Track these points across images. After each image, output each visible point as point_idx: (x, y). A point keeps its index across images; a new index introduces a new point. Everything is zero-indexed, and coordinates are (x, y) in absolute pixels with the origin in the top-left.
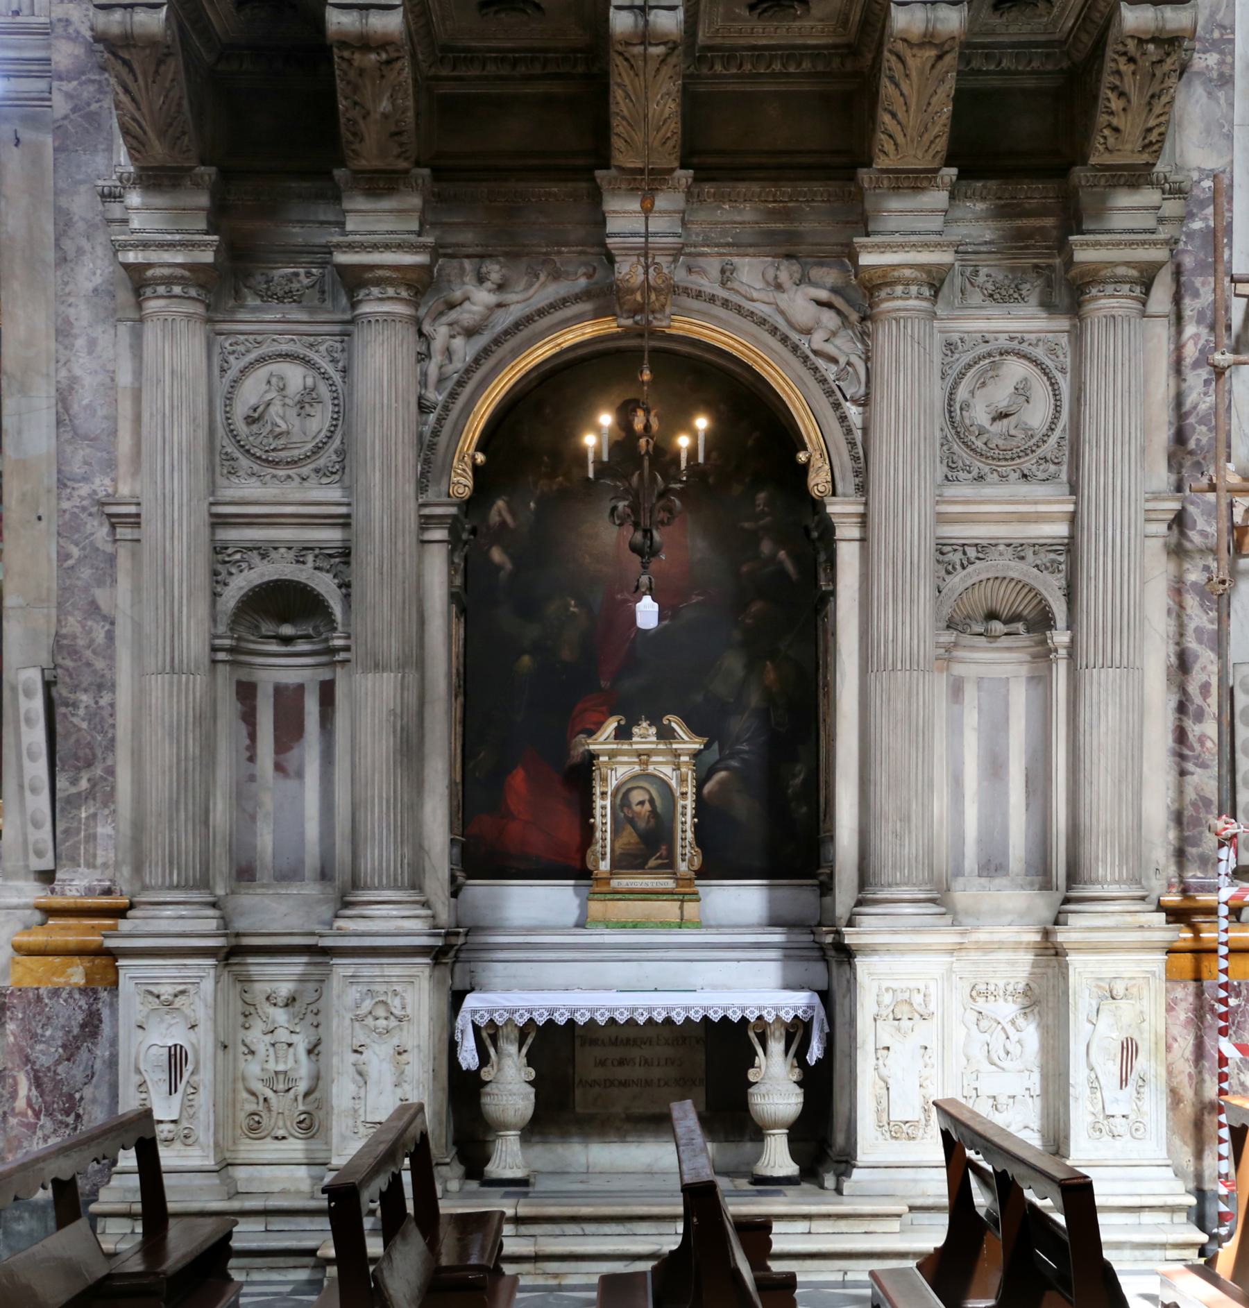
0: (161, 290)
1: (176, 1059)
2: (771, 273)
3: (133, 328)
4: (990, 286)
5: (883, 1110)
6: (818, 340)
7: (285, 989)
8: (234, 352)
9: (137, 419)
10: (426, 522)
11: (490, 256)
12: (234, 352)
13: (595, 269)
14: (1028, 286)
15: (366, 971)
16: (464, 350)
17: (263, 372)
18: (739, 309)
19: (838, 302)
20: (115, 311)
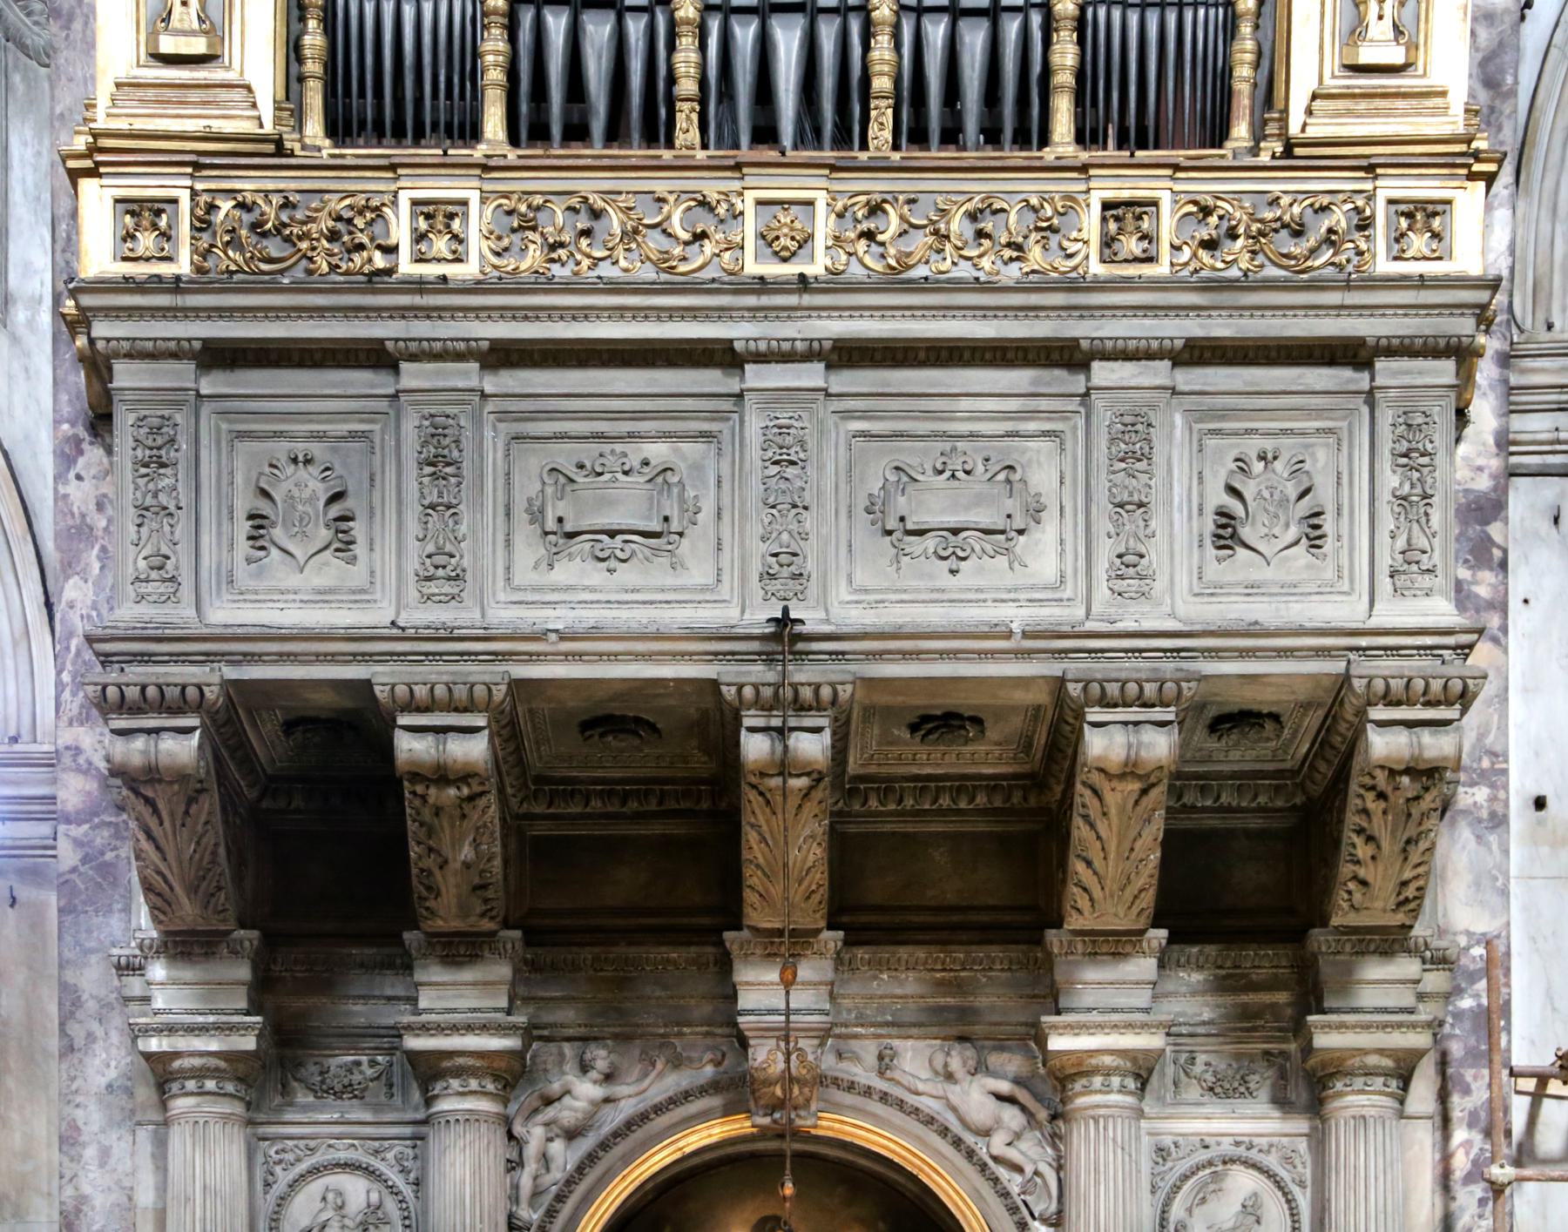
0: (191, 1085)
2: (939, 1060)
3: (155, 1132)
4: (1210, 1078)
6: (998, 1144)
8: (280, 1161)
11: (595, 1039)
12: (280, 1161)
13: (724, 1055)
14: (1256, 1077)
16: (564, 1156)
17: (316, 1187)
18: (900, 1104)
19: (1023, 1096)
20: (133, 1112)
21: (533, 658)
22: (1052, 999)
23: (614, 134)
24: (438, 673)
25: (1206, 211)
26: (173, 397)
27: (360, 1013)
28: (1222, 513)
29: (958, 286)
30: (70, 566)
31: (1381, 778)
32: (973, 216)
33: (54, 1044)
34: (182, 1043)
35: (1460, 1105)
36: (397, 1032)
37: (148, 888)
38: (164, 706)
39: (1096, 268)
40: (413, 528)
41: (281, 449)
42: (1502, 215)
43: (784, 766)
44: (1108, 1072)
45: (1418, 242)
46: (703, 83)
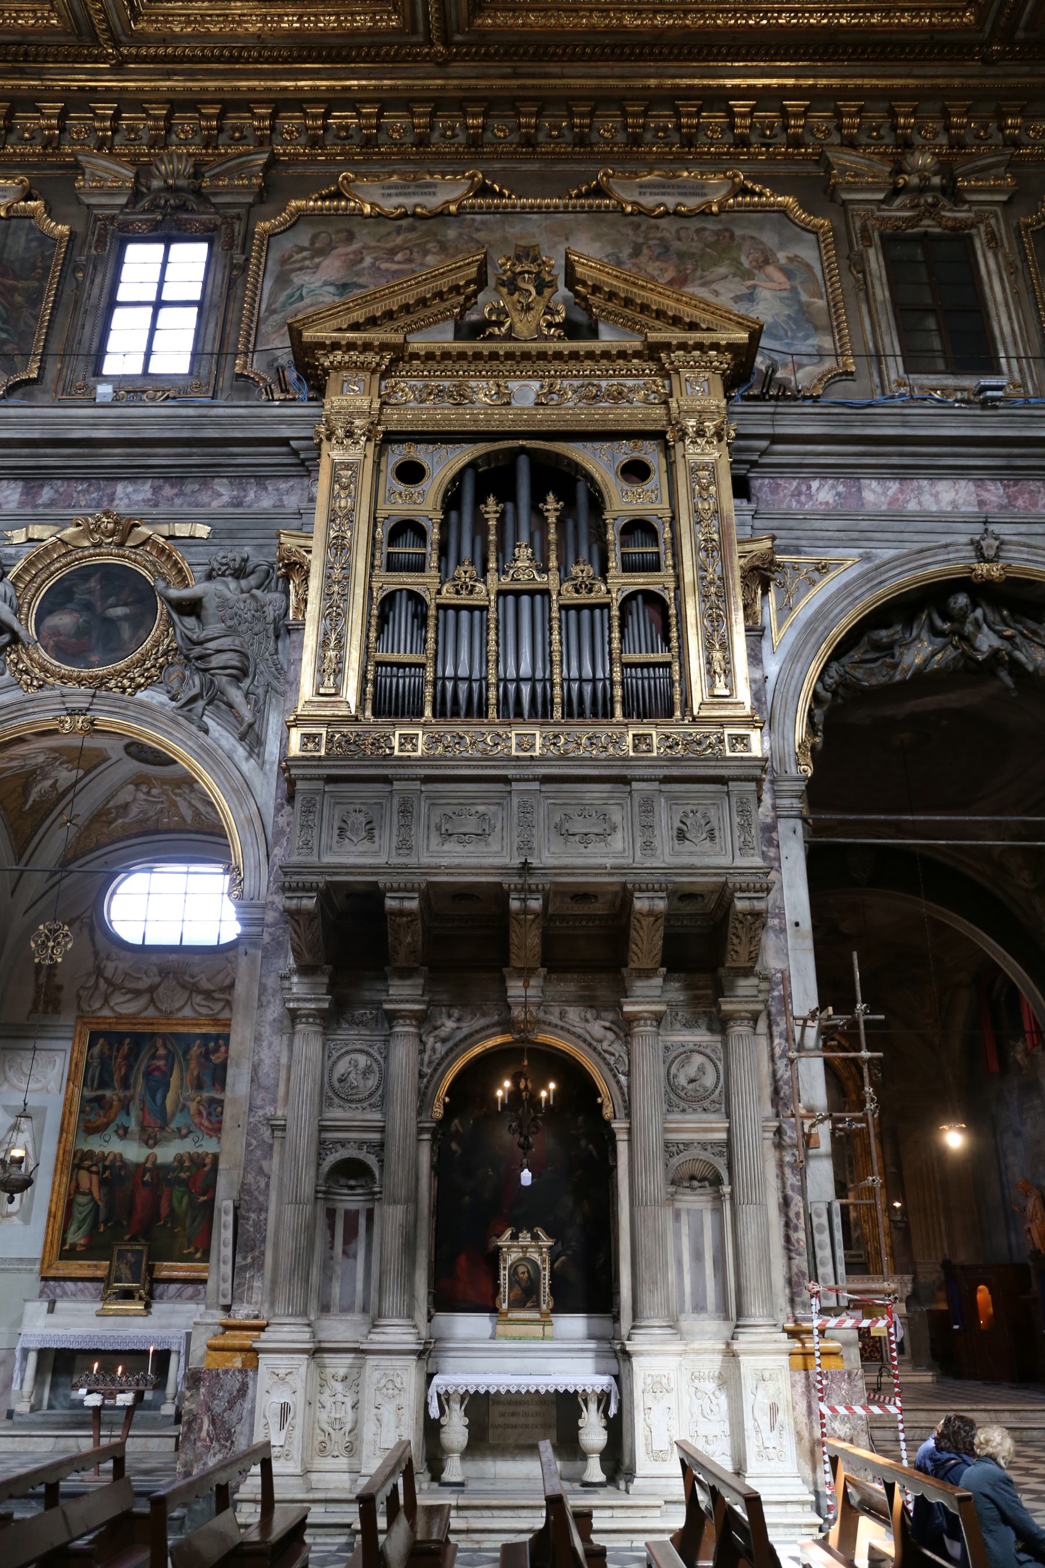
1: (285, 1410)
5: (649, 1444)
6: (605, 1045)
7: (342, 1372)
9: (288, 1080)
10: (421, 1131)
15: (383, 1363)
17: (347, 1058)
18: (568, 1031)
19: (614, 1028)
21: (436, 874)
22: (625, 992)
23: (468, 714)
24: (401, 879)
25: (668, 737)
26: (316, 792)
27: (367, 995)
28: (679, 829)
29: (585, 759)
30: (276, 844)
31: (740, 916)
32: (589, 738)
33: (255, 1004)
34: (302, 1005)
35: (776, 1030)
36: (381, 1002)
37: (294, 950)
38: (304, 889)
39: (631, 754)
40: (395, 832)
41: (351, 807)
42: (766, 738)
43: (526, 911)
44: (646, 1019)
45: (740, 747)
46: (498, 700)
